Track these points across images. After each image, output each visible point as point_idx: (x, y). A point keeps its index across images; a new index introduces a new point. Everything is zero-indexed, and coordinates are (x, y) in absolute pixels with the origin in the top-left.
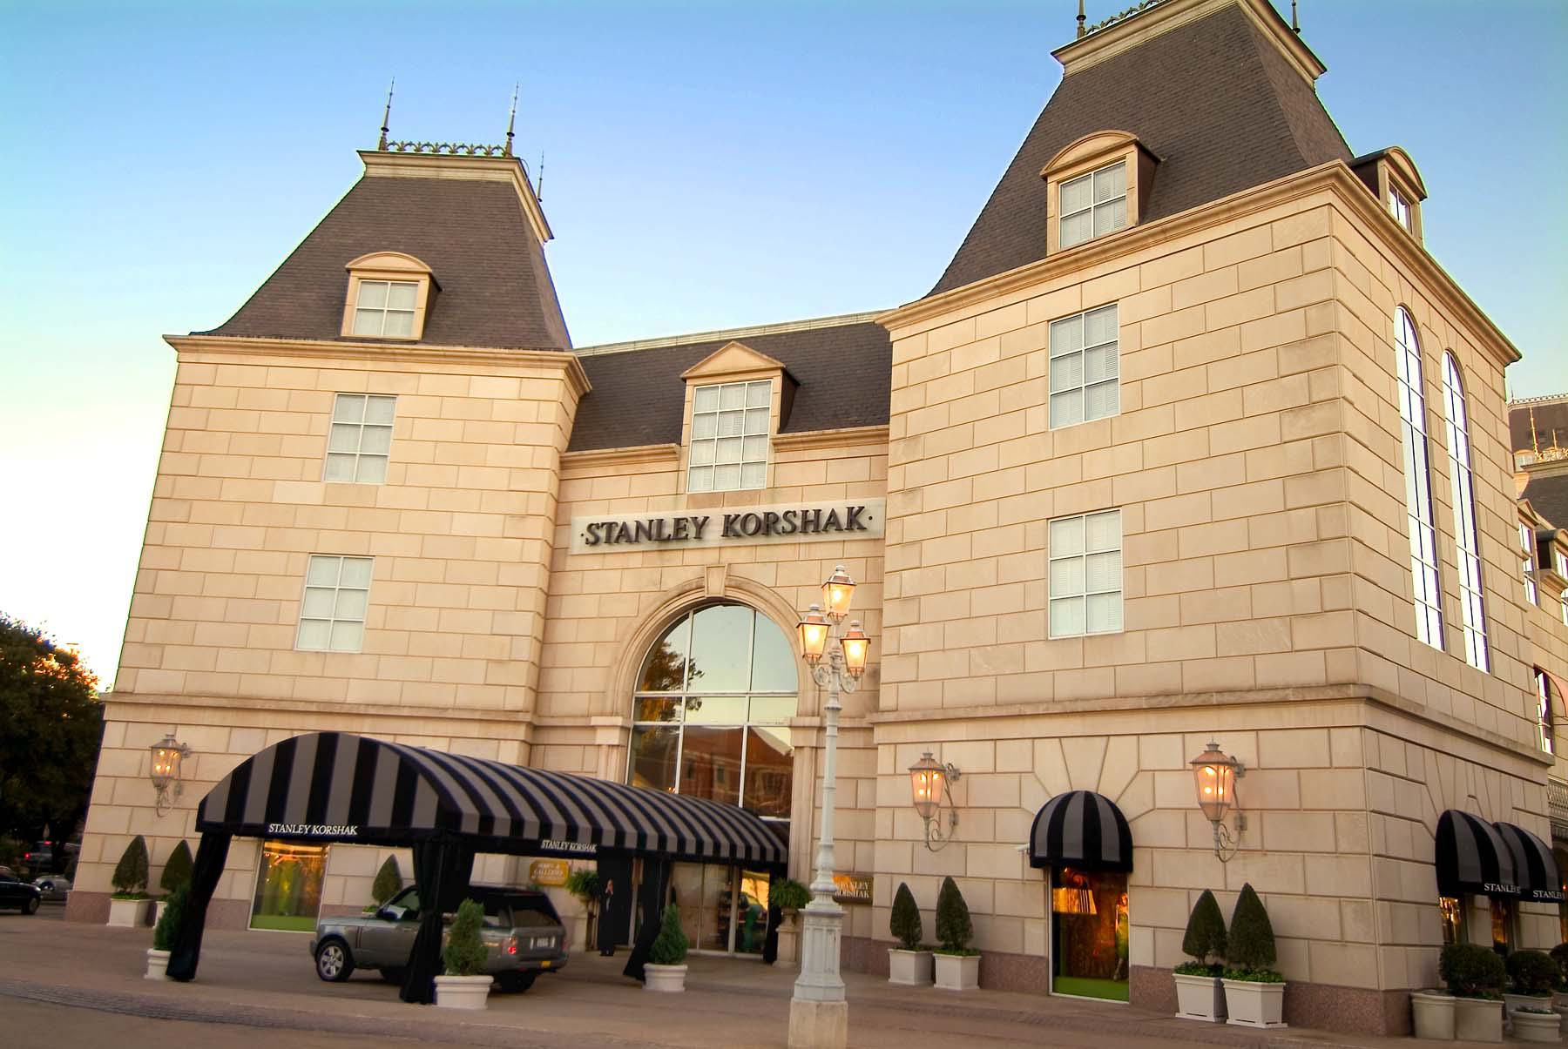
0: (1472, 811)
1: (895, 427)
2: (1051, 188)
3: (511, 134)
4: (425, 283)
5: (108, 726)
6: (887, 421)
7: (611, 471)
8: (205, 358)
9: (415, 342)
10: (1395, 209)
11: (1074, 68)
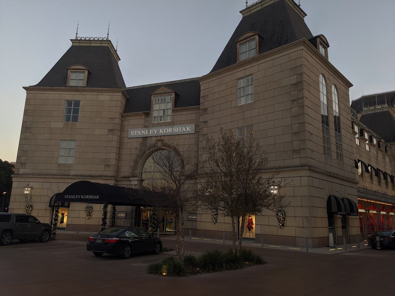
0: (337, 195)
1: (201, 107)
2: (238, 46)
3: (108, 34)
4: (87, 72)
5: (13, 182)
6: (200, 105)
7: (134, 118)
8: (33, 92)
9: (84, 87)
10: (322, 50)
11: (245, 15)
